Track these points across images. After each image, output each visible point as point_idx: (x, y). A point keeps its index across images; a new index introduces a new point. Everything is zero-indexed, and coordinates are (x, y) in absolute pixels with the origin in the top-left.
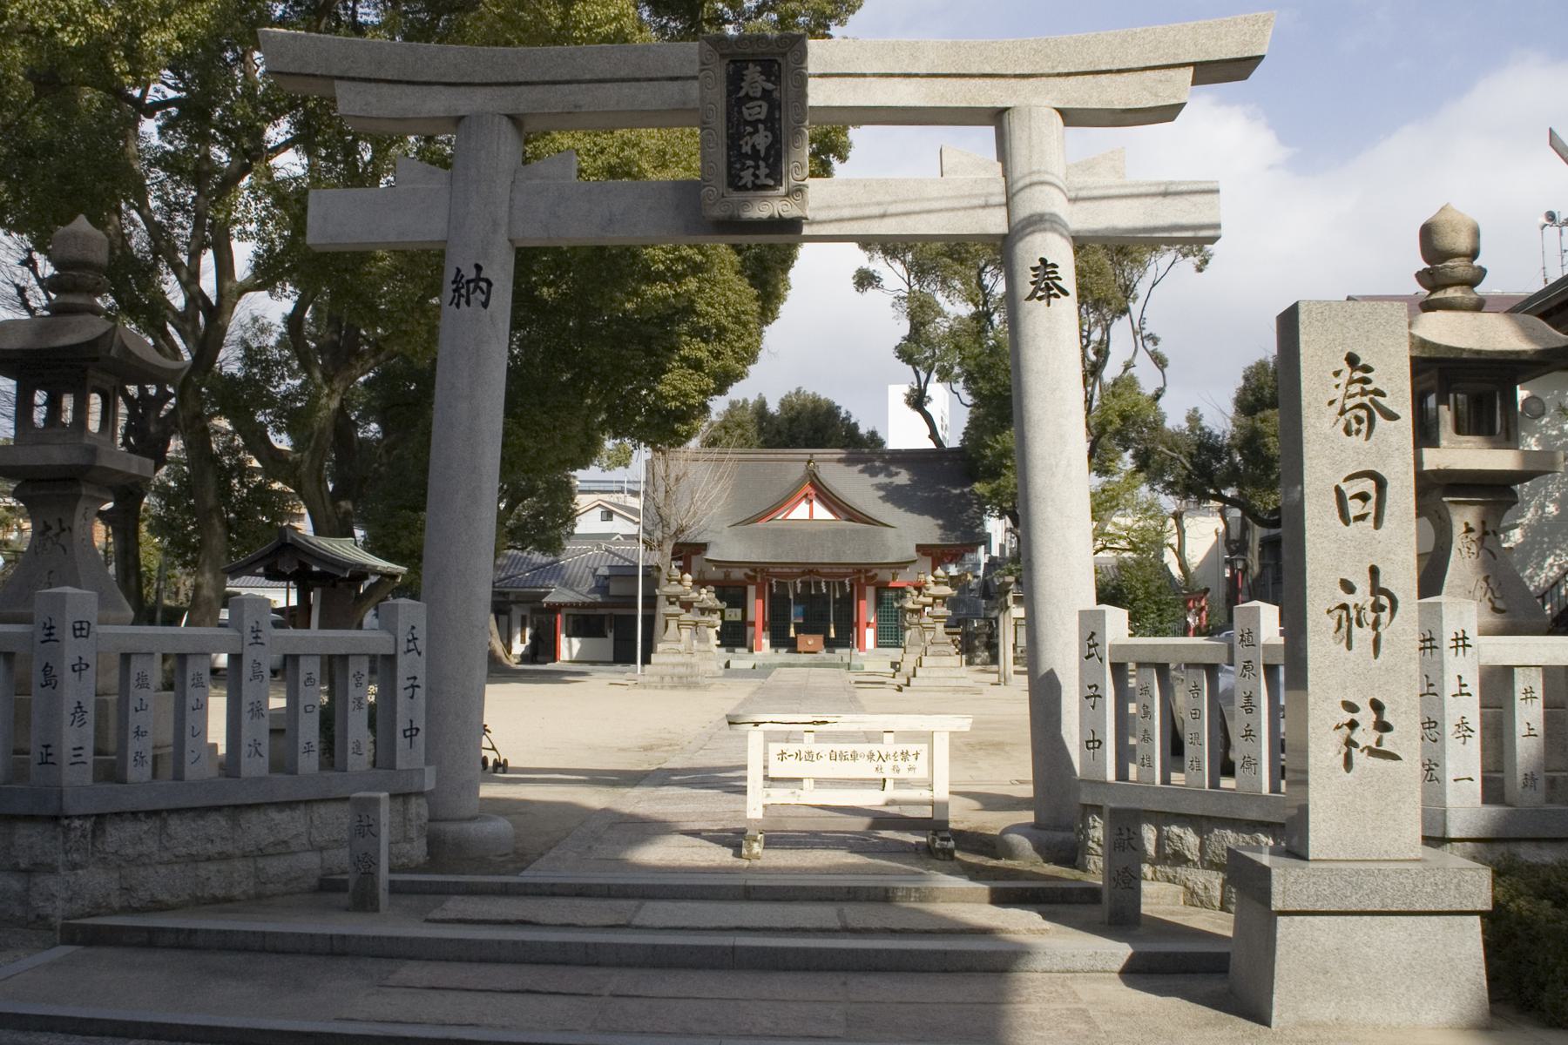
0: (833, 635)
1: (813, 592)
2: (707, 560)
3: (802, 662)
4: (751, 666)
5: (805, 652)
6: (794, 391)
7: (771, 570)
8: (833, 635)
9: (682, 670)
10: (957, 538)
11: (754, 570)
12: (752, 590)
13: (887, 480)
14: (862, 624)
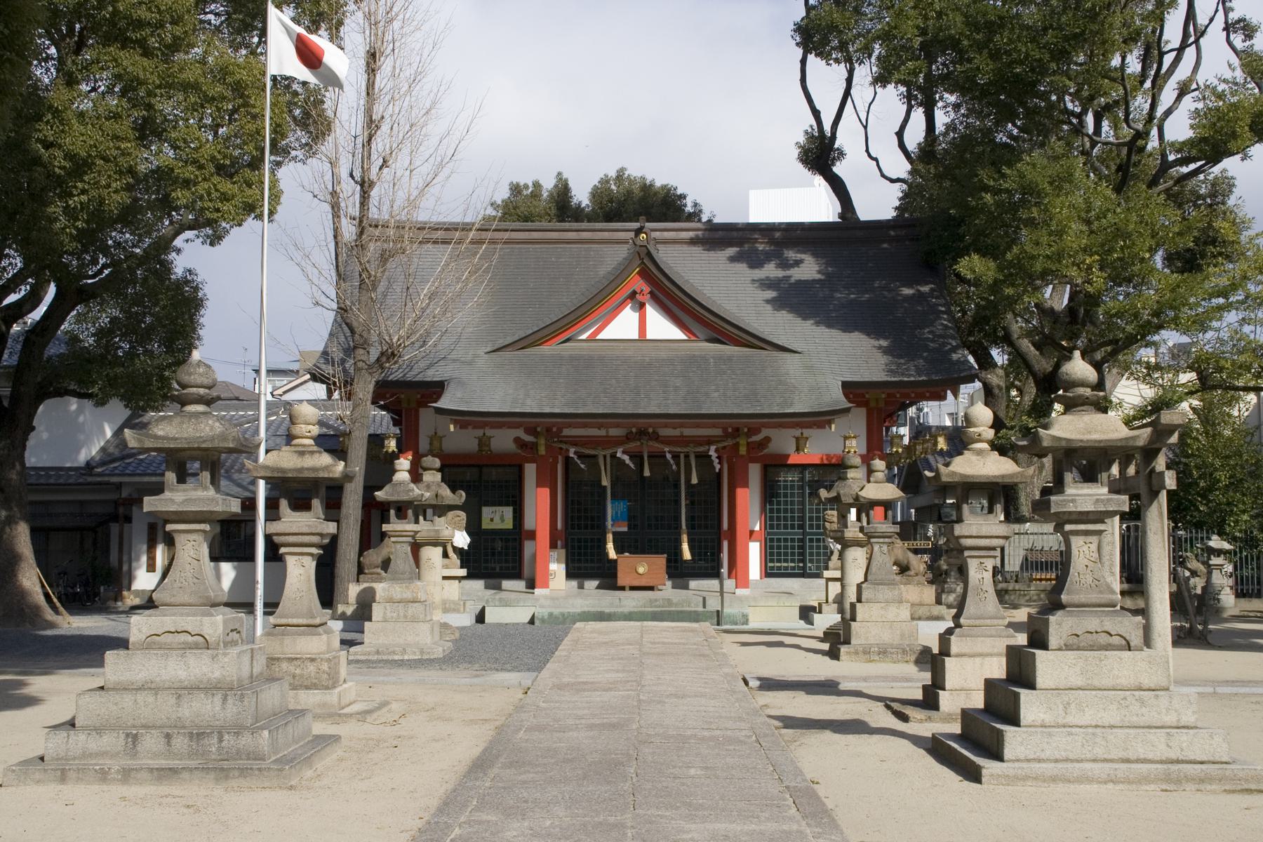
0: (687, 555)
1: (647, 473)
2: (440, 411)
3: (626, 610)
4: (527, 620)
5: (633, 588)
6: (612, 174)
7: (566, 432)
8: (687, 555)
9: (206, 708)
10: (919, 371)
11: (531, 431)
12: (530, 471)
13: (780, 273)
14: (741, 533)
